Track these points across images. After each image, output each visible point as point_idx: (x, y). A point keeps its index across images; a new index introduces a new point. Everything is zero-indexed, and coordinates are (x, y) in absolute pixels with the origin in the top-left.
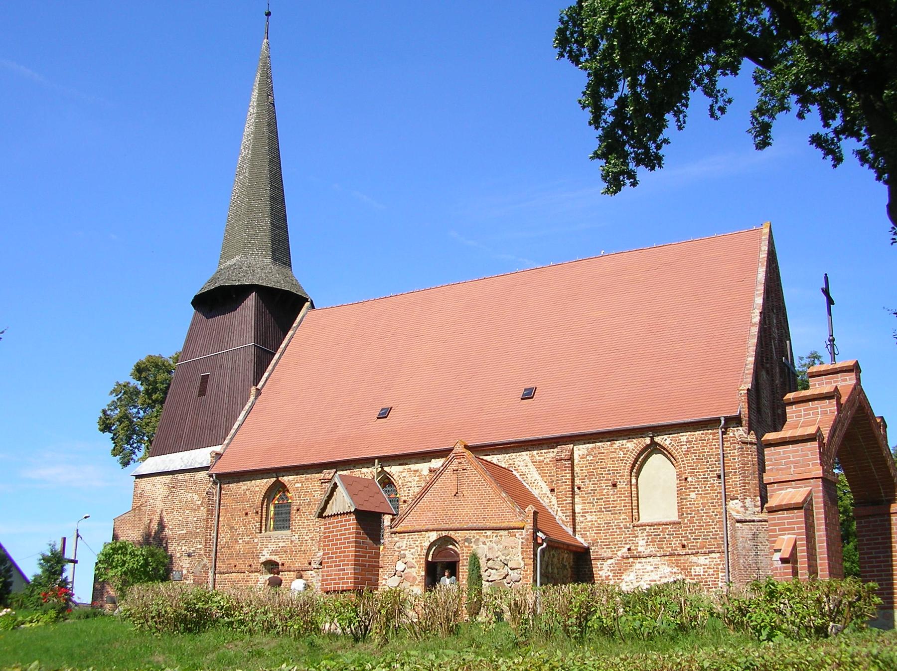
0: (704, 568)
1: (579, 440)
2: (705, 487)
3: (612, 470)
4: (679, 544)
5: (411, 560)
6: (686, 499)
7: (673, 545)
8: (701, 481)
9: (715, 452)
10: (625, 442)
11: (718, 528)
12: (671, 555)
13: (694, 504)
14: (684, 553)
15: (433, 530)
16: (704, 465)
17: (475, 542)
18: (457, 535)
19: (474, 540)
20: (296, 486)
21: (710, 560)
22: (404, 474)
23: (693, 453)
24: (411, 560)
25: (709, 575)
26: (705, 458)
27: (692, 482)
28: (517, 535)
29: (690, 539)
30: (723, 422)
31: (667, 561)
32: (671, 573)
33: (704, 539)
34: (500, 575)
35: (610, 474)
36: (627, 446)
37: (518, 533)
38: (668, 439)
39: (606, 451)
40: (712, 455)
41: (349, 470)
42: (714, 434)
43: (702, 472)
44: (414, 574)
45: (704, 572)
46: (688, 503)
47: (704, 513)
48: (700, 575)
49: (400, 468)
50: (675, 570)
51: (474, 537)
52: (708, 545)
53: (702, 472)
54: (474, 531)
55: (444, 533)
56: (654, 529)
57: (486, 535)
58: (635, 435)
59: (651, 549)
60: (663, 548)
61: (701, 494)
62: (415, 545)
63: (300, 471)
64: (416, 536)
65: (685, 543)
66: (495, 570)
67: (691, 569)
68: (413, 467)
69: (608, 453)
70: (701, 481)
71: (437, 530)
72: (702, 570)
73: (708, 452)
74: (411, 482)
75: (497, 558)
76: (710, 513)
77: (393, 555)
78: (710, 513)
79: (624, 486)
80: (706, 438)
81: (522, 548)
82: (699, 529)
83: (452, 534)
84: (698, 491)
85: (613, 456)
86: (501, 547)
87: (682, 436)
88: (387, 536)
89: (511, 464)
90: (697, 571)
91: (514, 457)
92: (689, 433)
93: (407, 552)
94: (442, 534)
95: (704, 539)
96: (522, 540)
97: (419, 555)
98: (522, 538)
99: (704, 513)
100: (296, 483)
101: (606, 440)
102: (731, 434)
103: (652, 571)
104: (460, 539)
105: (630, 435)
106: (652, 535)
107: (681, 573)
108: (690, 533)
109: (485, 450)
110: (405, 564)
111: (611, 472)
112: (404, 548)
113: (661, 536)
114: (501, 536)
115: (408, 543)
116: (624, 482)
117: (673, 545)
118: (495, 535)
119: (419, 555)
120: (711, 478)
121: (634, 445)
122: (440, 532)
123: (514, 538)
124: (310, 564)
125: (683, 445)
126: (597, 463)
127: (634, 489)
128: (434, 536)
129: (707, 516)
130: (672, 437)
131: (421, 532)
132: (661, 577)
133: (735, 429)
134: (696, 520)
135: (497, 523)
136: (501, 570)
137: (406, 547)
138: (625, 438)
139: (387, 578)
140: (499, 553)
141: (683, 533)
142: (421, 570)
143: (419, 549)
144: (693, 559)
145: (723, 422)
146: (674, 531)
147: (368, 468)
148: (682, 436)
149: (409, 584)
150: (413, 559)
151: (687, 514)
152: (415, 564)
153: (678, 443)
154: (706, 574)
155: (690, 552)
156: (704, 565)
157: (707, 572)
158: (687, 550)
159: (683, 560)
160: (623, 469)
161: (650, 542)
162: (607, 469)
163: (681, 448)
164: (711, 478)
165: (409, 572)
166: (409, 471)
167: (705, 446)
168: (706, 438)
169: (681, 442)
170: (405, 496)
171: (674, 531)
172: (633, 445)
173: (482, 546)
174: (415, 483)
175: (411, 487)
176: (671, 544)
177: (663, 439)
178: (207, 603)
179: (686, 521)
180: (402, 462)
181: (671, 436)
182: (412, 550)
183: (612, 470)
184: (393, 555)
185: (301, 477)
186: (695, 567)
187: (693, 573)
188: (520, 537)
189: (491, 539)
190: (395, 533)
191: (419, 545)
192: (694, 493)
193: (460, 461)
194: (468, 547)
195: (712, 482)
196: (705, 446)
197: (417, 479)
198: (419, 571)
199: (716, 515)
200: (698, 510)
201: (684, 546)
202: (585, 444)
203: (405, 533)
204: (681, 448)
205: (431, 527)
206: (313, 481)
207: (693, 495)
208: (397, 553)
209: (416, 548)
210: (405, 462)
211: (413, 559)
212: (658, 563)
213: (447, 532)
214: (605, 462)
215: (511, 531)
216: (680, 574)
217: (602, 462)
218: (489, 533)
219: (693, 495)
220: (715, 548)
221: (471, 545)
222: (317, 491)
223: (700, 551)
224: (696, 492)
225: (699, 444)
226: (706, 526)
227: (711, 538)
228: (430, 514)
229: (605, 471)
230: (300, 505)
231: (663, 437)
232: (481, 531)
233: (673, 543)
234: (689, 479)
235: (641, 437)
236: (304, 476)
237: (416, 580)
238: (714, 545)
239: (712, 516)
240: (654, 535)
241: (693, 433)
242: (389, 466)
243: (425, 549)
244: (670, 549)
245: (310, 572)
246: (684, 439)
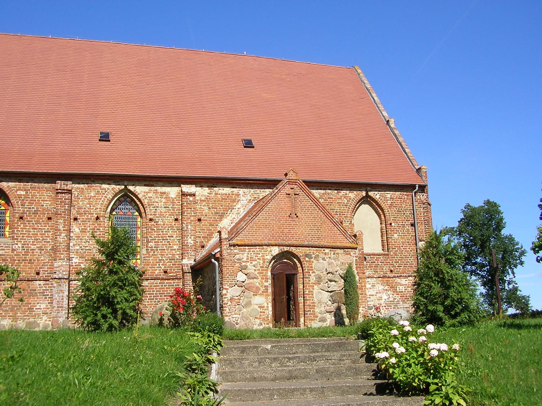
0: (405, 287)
1: (313, 186)
2: (403, 231)
3: (339, 212)
4: (388, 269)
5: (253, 271)
6: (392, 238)
7: (384, 270)
8: (401, 227)
9: (409, 207)
10: (348, 192)
11: (413, 260)
12: (384, 277)
13: (396, 242)
14: (393, 276)
15: (276, 245)
16: (402, 216)
17: (315, 258)
18: (298, 250)
19: (314, 256)
20: (18, 193)
21: (409, 282)
22: (150, 195)
23: (395, 207)
24: (253, 271)
25: (408, 292)
26: (403, 211)
27: (395, 226)
28: (352, 254)
29: (395, 267)
30: (417, 188)
31: (381, 281)
32: (384, 290)
33: (405, 267)
34: (339, 287)
35: (337, 214)
36: (349, 195)
37: (352, 252)
38: (378, 195)
39: (333, 197)
40: (407, 209)
41: (87, 184)
42: (407, 195)
43: (401, 220)
44: (257, 285)
45: (405, 290)
46: (393, 241)
47: (403, 249)
48: (403, 292)
49: (146, 189)
50: (386, 288)
51: (314, 253)
52: (407, 271)
53: (401, 220)
54: (314, 249)
55: (286, 249)
56: (371, 258)
57: (324, 252)
58: (354, 188)
59: (369, 272)
60: (377, 272)
61: (401, 236)
62: (257, 258)
63: (24, 179)
64: (258, 250)
65: (392, 269)
66: (334, 282)
67: (396, 287)
68: (160, 189)
69: (335, 198)
70: (401, 227)
71: (279, 245)
72: (404, 289)
73: (405, 207)
74: (158, 202)
75: (336, 272)
76: (407, 249)
77: (233, 267)
78: (407, 249)
79: (348, 224)
80: (403, 198)
81: (356, 265)
82: (401, 260)
83: (293, 249)
84: (399, 233)
85: (339, 201)
86: (339, 263)
87: (387, 194)
88: (225, 247)
89: (255, 198)
90: (401, 288)
91: (258, 192)
92: (392, 192)
93: (248, 264)
94: (284, 249)
95: (405, 267)
96: (356, 258)
97: (261, 267)
98: (356, 257)
99: (403, 249)
100: (17, 190)
101: (333, 188)
102: (418, 197)
103: (370, 288)
104: (301, 254)
105: (351, 188)
106: (369, 262)
107: (390, 290)
108: (395, 262)
109: (232, 183)
110: (246, 275)
111: (338, 213)
112: (245, 260)
113: (376, 263)
114: (338, 254)
115: (249, 255)
116: (348, 221)
117: (384, 270)
118: (333, 253)
119: (261, 267)
120: (407, 225)
121: (354, 195)
122: (282, 247)
123: (349, 256)
124: (38, 274)
125: (388, 200)
126: (327, 205)
127: (244, 228)
128: (276, 251)
129: (405, 251)
130: (381, 194)
131: (256, 246)
132: (377, 293)
133: (421, 194)
134: (399, 253)
135: (330, 242)
136: (340, 282)
137: (248, 259)
138: (347, 189)
139: (228, 287)
140: (338, 268)
141: (391, 262)
142: (264, 281)
143: (262, 262)
144: (398, 280)
145: (417, 188)
146: (384, 260)
147: (109, 184)
148: (387, 194)
149: (252, 293)
150: (255, 270)
151: (393, 249)
152: (258, 275)
153: (385, 198)
154: (407, 291)
155: (396, 275)
156: (405, 285)
157: (407, 289)
158: (394, 274)
159: (391, 281)
160: (347, 212)
161: (369, 267)
162: (335, 211)
163: (387, 202)
164: (407, 225)
165: (251, 283)
166: (156, 192)
167: (402, 203)
168: (403, 198)
169: (387, 198)
170: (151, 215)
171: (384, 260)
172: (354, 195)
173: (322, 261)
174: (162, 204)
175: (157, 207)
176: (383, 269)
177: (374, 194)
178: (417, 298)
179: (392, 254)
180: (147, 183)
181: (380, 192)
182: (254, 263)
183: (339, 212)
184: (233, 267)
185: (25, 185)
186: (399, 286)
187: (398, 290)
188: (354, 255)
189: (329, 256)
190: (234, 246)
191: (261, 258)
192: (396, 235)
193: (292, 187)
194: (309, 261)
195: (408, 228)
196: (402, 203)
197: (164, 200)
198: (262, 282)
199: (411, 251)
200: (400, 247)
201: (391, 271)
202: (317, 189)
203: (245, 246)
204: (387, 202)
205: (273, 242)
206: (40, 191)
207: (396, 236)
208: (237, 265)
209: (258, 260)
210: (152, 183)
211: (255, 270)
212: (374, 282)
213: (289, 248)
214: (333, 205)
215: (347, 250)
216: (390, 291)
217: (331, 205)
218: (327, 250)
219: (396, 236)
220: (412, 273)
221: (312, 260)
222: (47, 201)
223: (402, 275)
224: (398, 234)
225: (398, 201)
226: (405, 258)
227: (409, 266)
228: (266, 231)
229: (334, 212)
230: (24, 213)
231: (374, 192)
232: (320, 249)
233: (384, 268)
234: (393, 224)
235: (359, 190)
236: (30, 184)
237: (259, 289)
238: (411, 271)
239: (409, 251)
240: (371, 262)
241: (394, 193)
242: (133, 185)
243: (267, 262)
244: (382, 273)
245: (38, 282)
246: (389, 196)
